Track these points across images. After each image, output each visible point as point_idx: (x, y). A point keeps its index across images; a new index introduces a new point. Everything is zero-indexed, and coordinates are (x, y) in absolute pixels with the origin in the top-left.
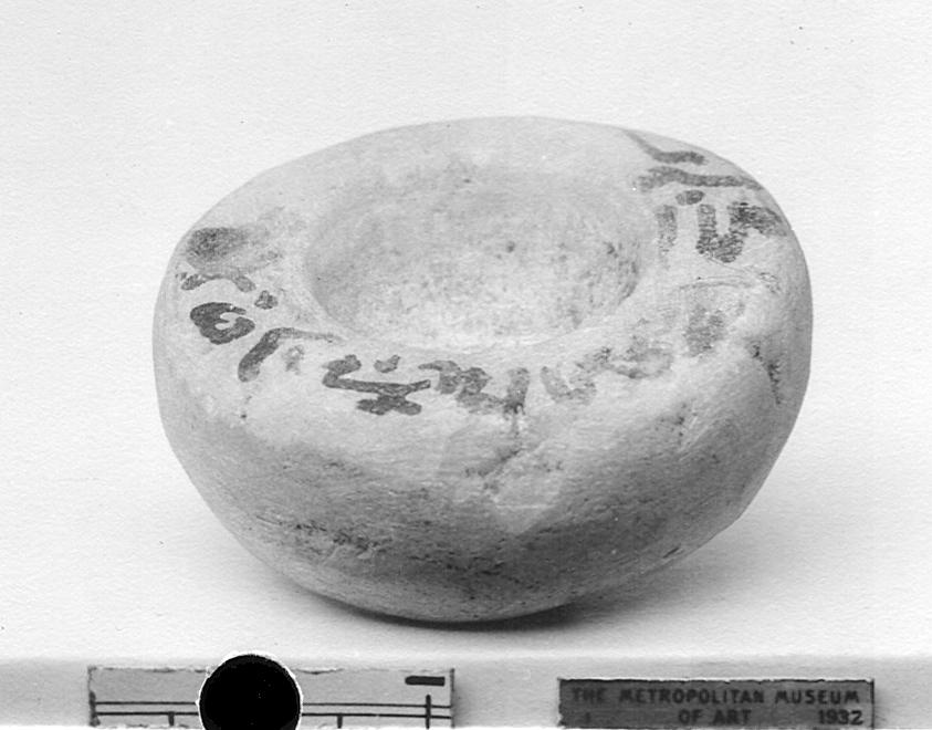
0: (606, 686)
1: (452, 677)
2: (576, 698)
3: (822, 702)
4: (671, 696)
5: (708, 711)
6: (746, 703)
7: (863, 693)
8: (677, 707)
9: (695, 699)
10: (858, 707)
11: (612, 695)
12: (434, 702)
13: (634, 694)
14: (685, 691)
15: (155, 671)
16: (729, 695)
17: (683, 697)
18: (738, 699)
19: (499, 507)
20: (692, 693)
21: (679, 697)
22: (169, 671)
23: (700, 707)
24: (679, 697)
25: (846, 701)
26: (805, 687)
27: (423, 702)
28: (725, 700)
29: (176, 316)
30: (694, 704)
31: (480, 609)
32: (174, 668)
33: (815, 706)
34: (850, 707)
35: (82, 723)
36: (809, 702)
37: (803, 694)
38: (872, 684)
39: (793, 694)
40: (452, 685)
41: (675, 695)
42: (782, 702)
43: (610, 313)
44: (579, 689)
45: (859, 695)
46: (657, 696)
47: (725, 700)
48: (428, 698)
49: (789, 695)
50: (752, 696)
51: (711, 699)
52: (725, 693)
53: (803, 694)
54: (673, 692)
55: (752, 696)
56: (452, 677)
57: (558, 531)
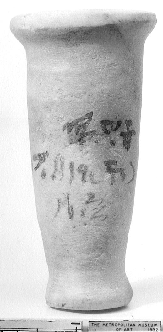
0: (99, 322)
1: (82, 323)
2: (93, 325)
3: (149, 326)
4: (114, 325)
5: (123, 328)
8: (116, 328)
9: (120, 325)
10: (157, 328)
11: (101, 324)
12: (77, 329)
16: (127, 325)
17: (115, 325)
18: (129, 325)
21: (116, 325)
22: (17, 321)
23: (121, 327)
24: (116, 325)
25: (154, 326)
27: (75, 329)
28: (127, 325)
29: (103, 84)
30: (119, 327)
33: (147, 327)
34: (155, 327)
35: (147, 330)
39: (142, 324)
40: (82, 324)
41: (115, 325)
42: (140, 326)
44: (93, 324)
46: (111, 325)
47: (127, 325)
48: (76, 328)
49: (141, 325)
50: (133, 325)
52: (127, 324)
53: (145, 325)
55: (133, 325)
56: (82, 323)
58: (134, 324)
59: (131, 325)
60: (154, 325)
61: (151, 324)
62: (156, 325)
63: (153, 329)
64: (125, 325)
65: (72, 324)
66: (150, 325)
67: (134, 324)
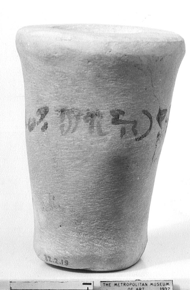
2: (104, 285)
3: (160, 285)
4: (126, 285)
6: (143, 286)
7: (170, 283)
9: (131, 285)
10: (169, 287)
11: (112, 284)
13: (117, 284)
14: (129, 283)
15: (25, 282)
16: (139, 284)
17: (127, 284)
19: (92, 92)
20: (131, 284)
21: (128, 285)
24: (128, 285)
26: (157, 282)
31: (127, 139)
32: (30, 281)
36: (158, 286)
37: (157, 284)
38: (172, 281)
41: (127, 284)
43: (109, 64)
45: (169, 283)
46: (123, 284)
48: (88, 288)
49: (153, 284)
51: (135, 285)
52: (138, 284)
53: (157, 284)
54: (126, 284)
55: (145, 285)
57: (174, 70)
58: (146, 284)
59: (143, 285)
60: (166, 284)
61: (163, 284)
62: (167, 284)
63: (165, 288)
64: (137, 285)
65: (84, 284)
66: (162, 284)
67: (146, 284)
